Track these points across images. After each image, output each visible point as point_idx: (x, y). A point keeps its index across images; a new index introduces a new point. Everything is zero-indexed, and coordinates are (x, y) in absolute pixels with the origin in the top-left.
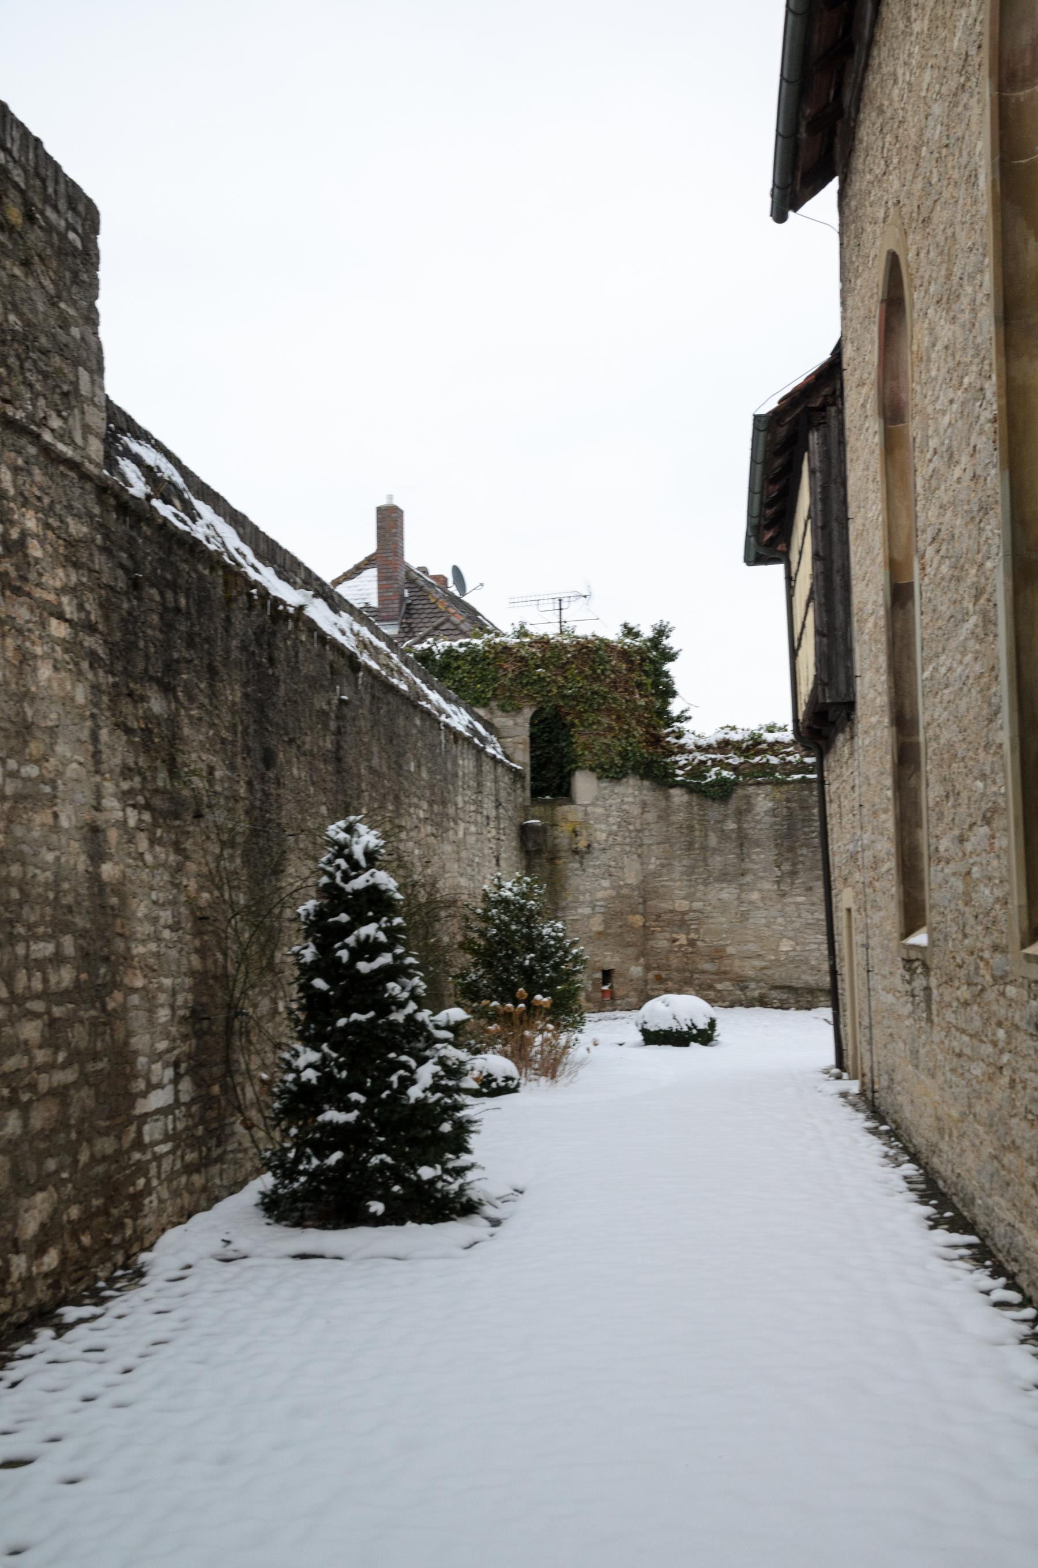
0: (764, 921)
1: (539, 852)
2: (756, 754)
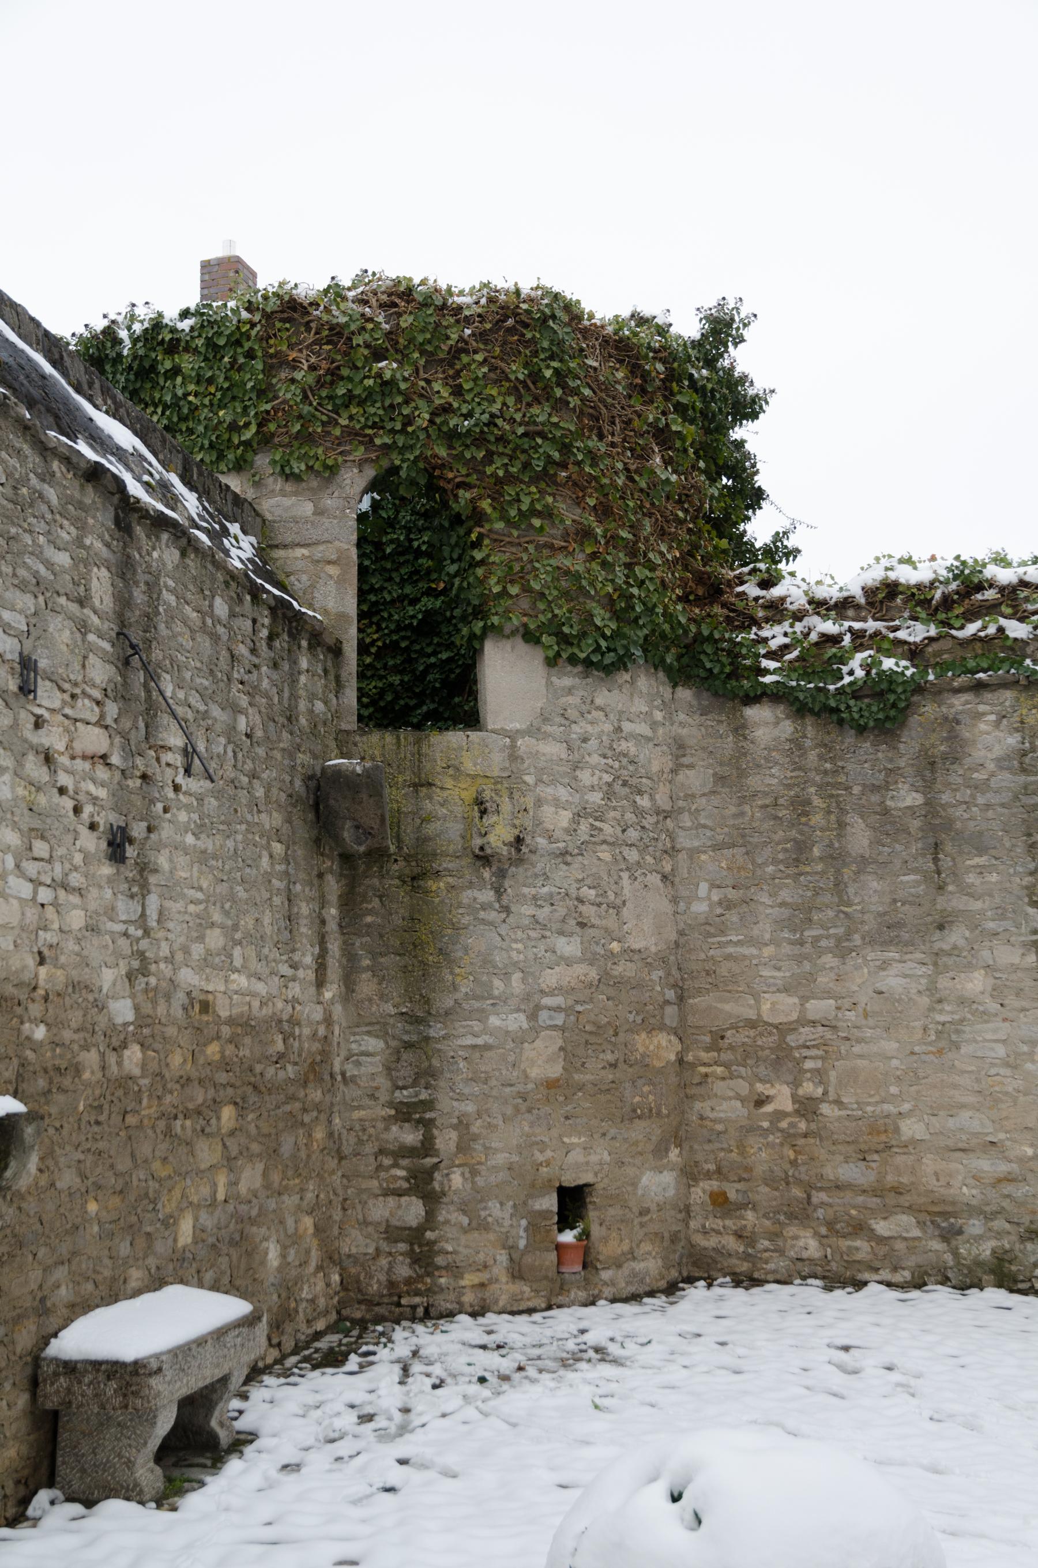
0: (1001, 1051)
1: (378, 855)
2: (970, 616)
